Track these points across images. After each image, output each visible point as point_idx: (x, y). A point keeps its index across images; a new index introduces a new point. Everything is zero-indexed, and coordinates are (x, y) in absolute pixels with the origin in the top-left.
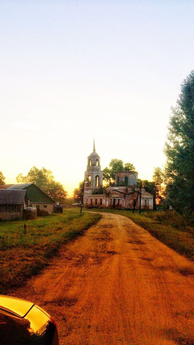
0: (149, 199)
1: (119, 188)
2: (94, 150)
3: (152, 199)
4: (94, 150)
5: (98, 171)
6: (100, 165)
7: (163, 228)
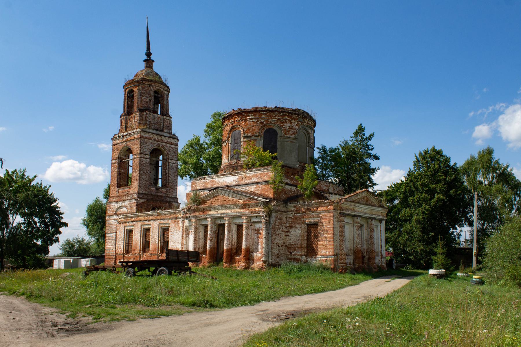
0: (374, 222)
1: (241, 179)
2: (149, 62)
3: (380, 221)
4: (149, 62)
5: (163, 131)
6: (171, 113)
7: (333, 311)
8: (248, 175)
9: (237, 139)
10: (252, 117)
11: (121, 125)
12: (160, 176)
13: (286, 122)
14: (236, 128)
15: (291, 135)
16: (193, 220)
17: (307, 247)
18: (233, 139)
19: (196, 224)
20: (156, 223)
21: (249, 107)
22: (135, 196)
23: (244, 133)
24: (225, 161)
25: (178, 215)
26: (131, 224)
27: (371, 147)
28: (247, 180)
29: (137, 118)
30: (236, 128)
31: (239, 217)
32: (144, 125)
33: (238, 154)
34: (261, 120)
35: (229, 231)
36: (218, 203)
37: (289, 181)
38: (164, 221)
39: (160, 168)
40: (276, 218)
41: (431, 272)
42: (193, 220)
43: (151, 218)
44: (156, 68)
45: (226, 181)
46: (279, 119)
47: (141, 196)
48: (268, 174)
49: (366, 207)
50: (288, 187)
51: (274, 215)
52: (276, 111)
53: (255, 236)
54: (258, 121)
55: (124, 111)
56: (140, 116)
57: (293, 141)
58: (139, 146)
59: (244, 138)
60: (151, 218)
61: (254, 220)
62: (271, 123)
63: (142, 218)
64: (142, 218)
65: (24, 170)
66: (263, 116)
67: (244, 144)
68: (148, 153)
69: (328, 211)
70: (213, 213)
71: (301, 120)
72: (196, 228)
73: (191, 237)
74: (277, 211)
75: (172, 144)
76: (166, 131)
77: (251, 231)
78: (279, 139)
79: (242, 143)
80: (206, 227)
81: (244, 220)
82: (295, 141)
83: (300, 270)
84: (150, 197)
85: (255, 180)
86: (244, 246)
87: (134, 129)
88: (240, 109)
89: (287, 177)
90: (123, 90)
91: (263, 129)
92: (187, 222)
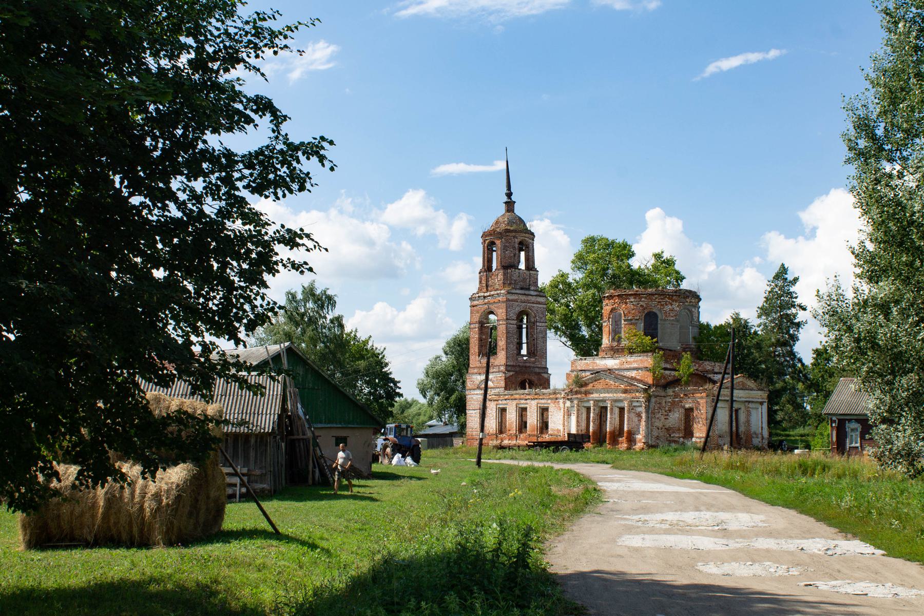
5: (529, 289)
11: (480, 282)
12: (524, 340)
16: (576, 402)
17: (686, 429)
19: (578, 405)
20: (534, 403)
22: (502, 368)
24: (606, 341)
25: (558, 396)
26: (504, 402)
27: (794, 295)
29: (500, 277)
31: (621, 401)
32: (510, 284)
33: (620, 338)
34: (641, 303)
35: (611, 414)
36: (600, 387)
37: (668, 366)
38: (543, 401)
39: (524, 331)
40: (656, 402)
41: (796, 451)
42: (576, 402)
43: (528, 397)
44: (518, 210)
47: (509, 368)
48: (648, 361)
49: (741, 391)
50: (667, 372)
51: (653, 400)
53: (636, 419)
55: (484, 266)
56: (504, 274)
58: (504, 310)
60: (528, 397)
61: (635, 404)
63: (517, 396)
64: (517, 396)
65: (356, 331)
68: (515, 317)
69: (702, 398)
70: (595, 396)
72: (578, 410)
73: (574, 418)
74: (656, 397)
75: (539, 303)
76: (532, 288)
77: (632, 415)
80: (588, 409)
81: (625, 404)
83: (676, 450)
84: (518, 369)
85: (635, 365)
86: (626, 429)
87: (497, 290)
89: (666, 362)
90: (481, 240)
92: (568, 404)
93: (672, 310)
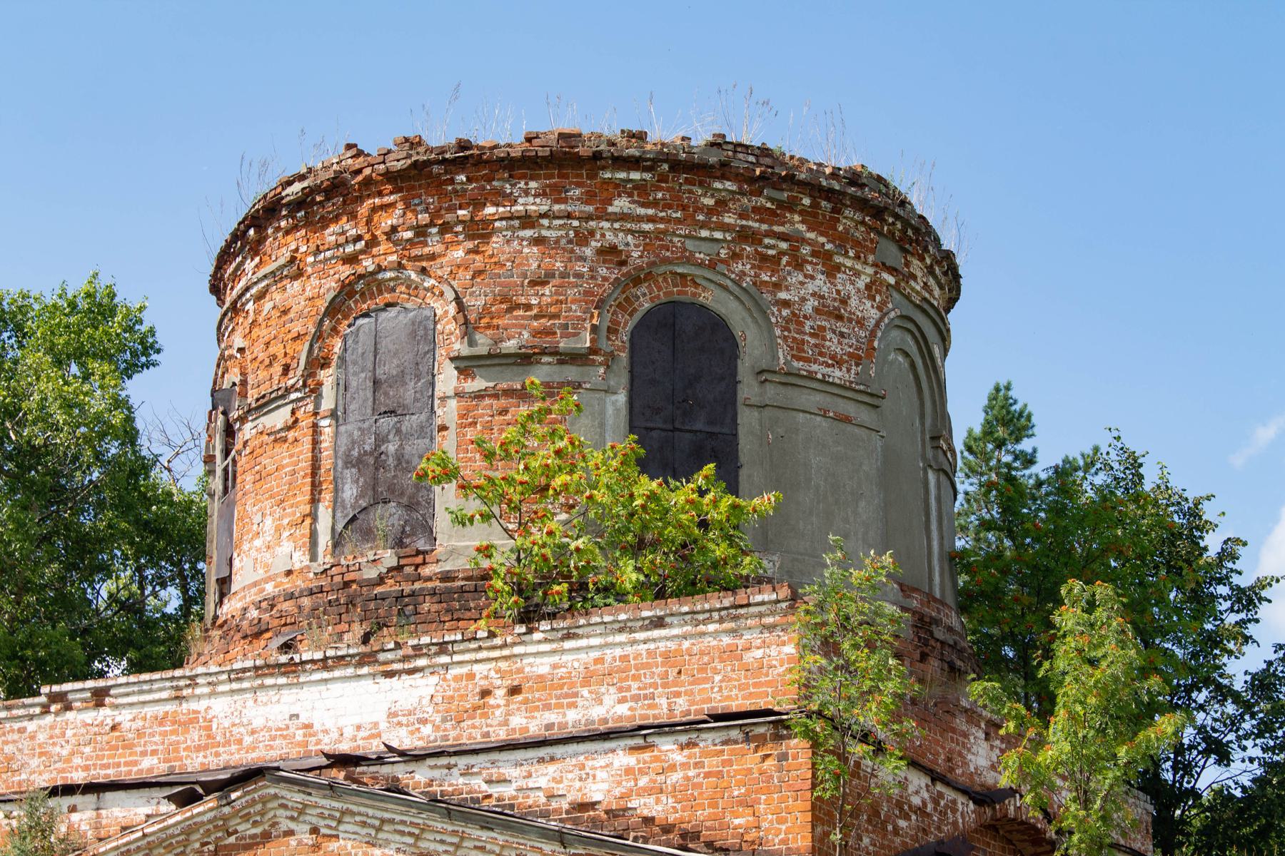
8: (542, 666)
9: (400, 379)
10: (529, 205)
13: (798, 264)
14: (381, 287)
15: (839, 363)
18: (359, 381)
21: (502, 130)
23: (468, 328)
28: (531, 708)
30: (381, 287)
34: (608, 233)
45: (320, 719)
46: (745, 236)
48: (762, 656)
52: (724, 169)
54: (583, 238)
57: (850, 409)
59: (466, 366)
62: (689, 260)
66: (620, 204)
67: (467, 419)
71: (891, 253)
78: (748, 389)
79: (448, 412)
82: (864, 415)
85: (610, 708)
88: (413, 143)
91: (626, 305)
93: (834, 311)
